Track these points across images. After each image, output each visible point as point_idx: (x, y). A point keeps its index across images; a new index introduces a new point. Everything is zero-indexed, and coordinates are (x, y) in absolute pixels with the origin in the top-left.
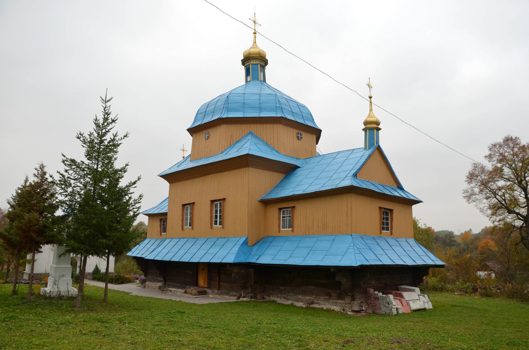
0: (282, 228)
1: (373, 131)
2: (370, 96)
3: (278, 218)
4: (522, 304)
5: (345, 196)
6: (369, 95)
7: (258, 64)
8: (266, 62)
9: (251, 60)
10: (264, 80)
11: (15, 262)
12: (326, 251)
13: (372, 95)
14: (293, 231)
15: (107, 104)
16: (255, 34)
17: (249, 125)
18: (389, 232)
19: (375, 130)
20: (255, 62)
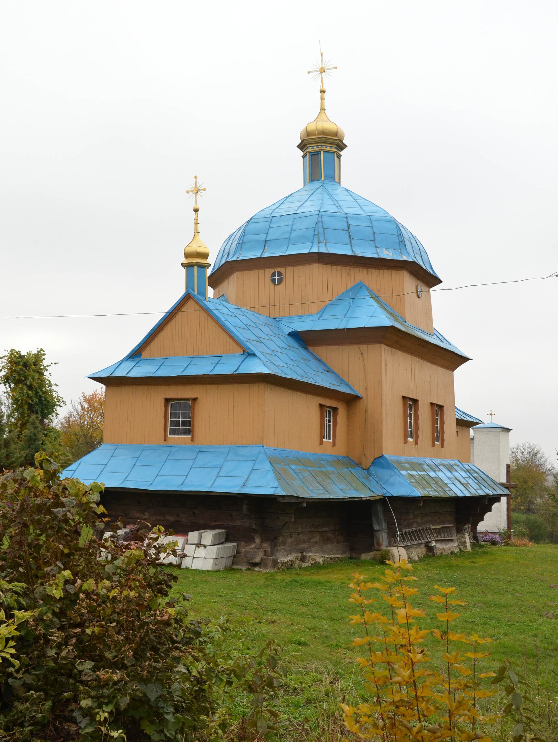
0: (170, 435)
1: (192, 268)
2: (197, 207)
3: (163, 415)
4: (340, 570)
5: (262, 386)
6: (193, 206)
7: (334, 153)
8: (341, 146)
9: (323, 144)
10: (339, 183)
11: (327, 529)
12: (220, 474)
13: (199, 206)
14: (192, 440)
15: (288, 237)
16: (323, 93)
17: (292, 268)
18: (190, 436)
19: (196, 267)
20: (328, 149)
